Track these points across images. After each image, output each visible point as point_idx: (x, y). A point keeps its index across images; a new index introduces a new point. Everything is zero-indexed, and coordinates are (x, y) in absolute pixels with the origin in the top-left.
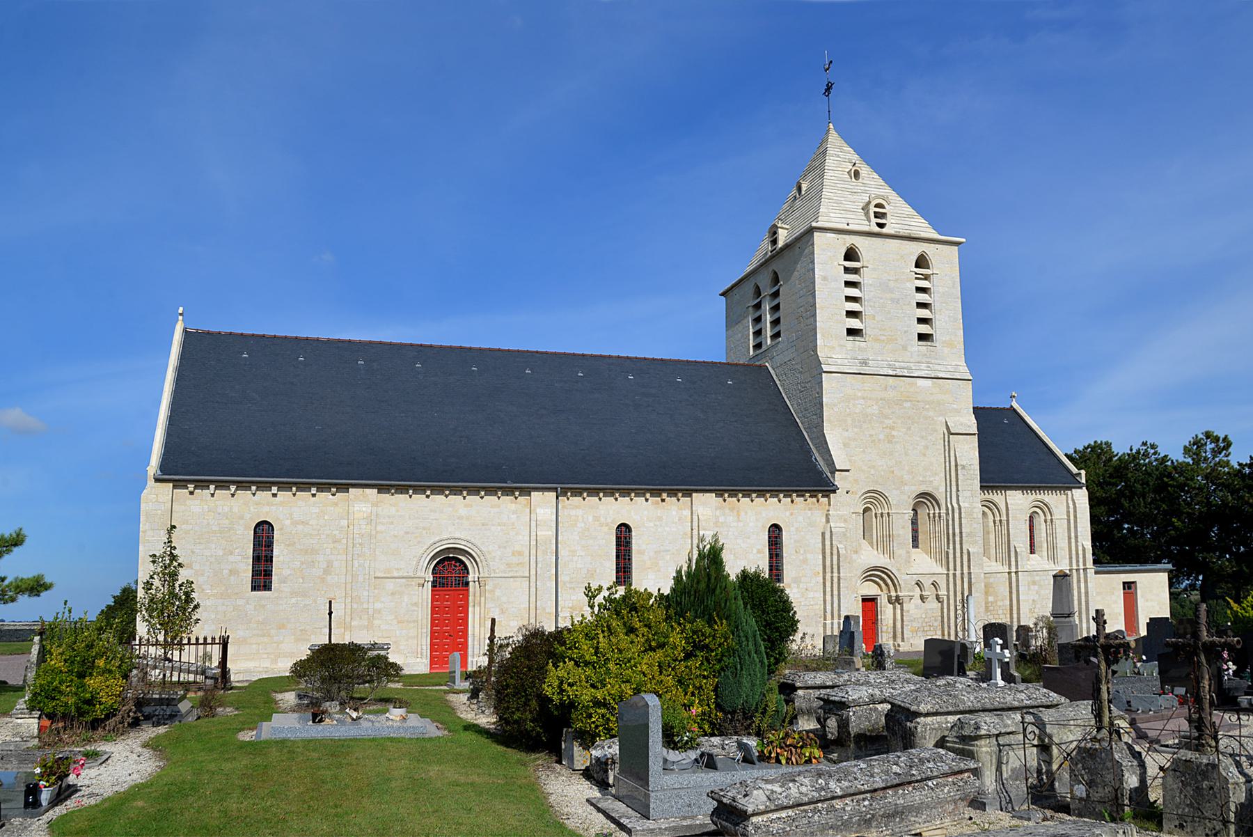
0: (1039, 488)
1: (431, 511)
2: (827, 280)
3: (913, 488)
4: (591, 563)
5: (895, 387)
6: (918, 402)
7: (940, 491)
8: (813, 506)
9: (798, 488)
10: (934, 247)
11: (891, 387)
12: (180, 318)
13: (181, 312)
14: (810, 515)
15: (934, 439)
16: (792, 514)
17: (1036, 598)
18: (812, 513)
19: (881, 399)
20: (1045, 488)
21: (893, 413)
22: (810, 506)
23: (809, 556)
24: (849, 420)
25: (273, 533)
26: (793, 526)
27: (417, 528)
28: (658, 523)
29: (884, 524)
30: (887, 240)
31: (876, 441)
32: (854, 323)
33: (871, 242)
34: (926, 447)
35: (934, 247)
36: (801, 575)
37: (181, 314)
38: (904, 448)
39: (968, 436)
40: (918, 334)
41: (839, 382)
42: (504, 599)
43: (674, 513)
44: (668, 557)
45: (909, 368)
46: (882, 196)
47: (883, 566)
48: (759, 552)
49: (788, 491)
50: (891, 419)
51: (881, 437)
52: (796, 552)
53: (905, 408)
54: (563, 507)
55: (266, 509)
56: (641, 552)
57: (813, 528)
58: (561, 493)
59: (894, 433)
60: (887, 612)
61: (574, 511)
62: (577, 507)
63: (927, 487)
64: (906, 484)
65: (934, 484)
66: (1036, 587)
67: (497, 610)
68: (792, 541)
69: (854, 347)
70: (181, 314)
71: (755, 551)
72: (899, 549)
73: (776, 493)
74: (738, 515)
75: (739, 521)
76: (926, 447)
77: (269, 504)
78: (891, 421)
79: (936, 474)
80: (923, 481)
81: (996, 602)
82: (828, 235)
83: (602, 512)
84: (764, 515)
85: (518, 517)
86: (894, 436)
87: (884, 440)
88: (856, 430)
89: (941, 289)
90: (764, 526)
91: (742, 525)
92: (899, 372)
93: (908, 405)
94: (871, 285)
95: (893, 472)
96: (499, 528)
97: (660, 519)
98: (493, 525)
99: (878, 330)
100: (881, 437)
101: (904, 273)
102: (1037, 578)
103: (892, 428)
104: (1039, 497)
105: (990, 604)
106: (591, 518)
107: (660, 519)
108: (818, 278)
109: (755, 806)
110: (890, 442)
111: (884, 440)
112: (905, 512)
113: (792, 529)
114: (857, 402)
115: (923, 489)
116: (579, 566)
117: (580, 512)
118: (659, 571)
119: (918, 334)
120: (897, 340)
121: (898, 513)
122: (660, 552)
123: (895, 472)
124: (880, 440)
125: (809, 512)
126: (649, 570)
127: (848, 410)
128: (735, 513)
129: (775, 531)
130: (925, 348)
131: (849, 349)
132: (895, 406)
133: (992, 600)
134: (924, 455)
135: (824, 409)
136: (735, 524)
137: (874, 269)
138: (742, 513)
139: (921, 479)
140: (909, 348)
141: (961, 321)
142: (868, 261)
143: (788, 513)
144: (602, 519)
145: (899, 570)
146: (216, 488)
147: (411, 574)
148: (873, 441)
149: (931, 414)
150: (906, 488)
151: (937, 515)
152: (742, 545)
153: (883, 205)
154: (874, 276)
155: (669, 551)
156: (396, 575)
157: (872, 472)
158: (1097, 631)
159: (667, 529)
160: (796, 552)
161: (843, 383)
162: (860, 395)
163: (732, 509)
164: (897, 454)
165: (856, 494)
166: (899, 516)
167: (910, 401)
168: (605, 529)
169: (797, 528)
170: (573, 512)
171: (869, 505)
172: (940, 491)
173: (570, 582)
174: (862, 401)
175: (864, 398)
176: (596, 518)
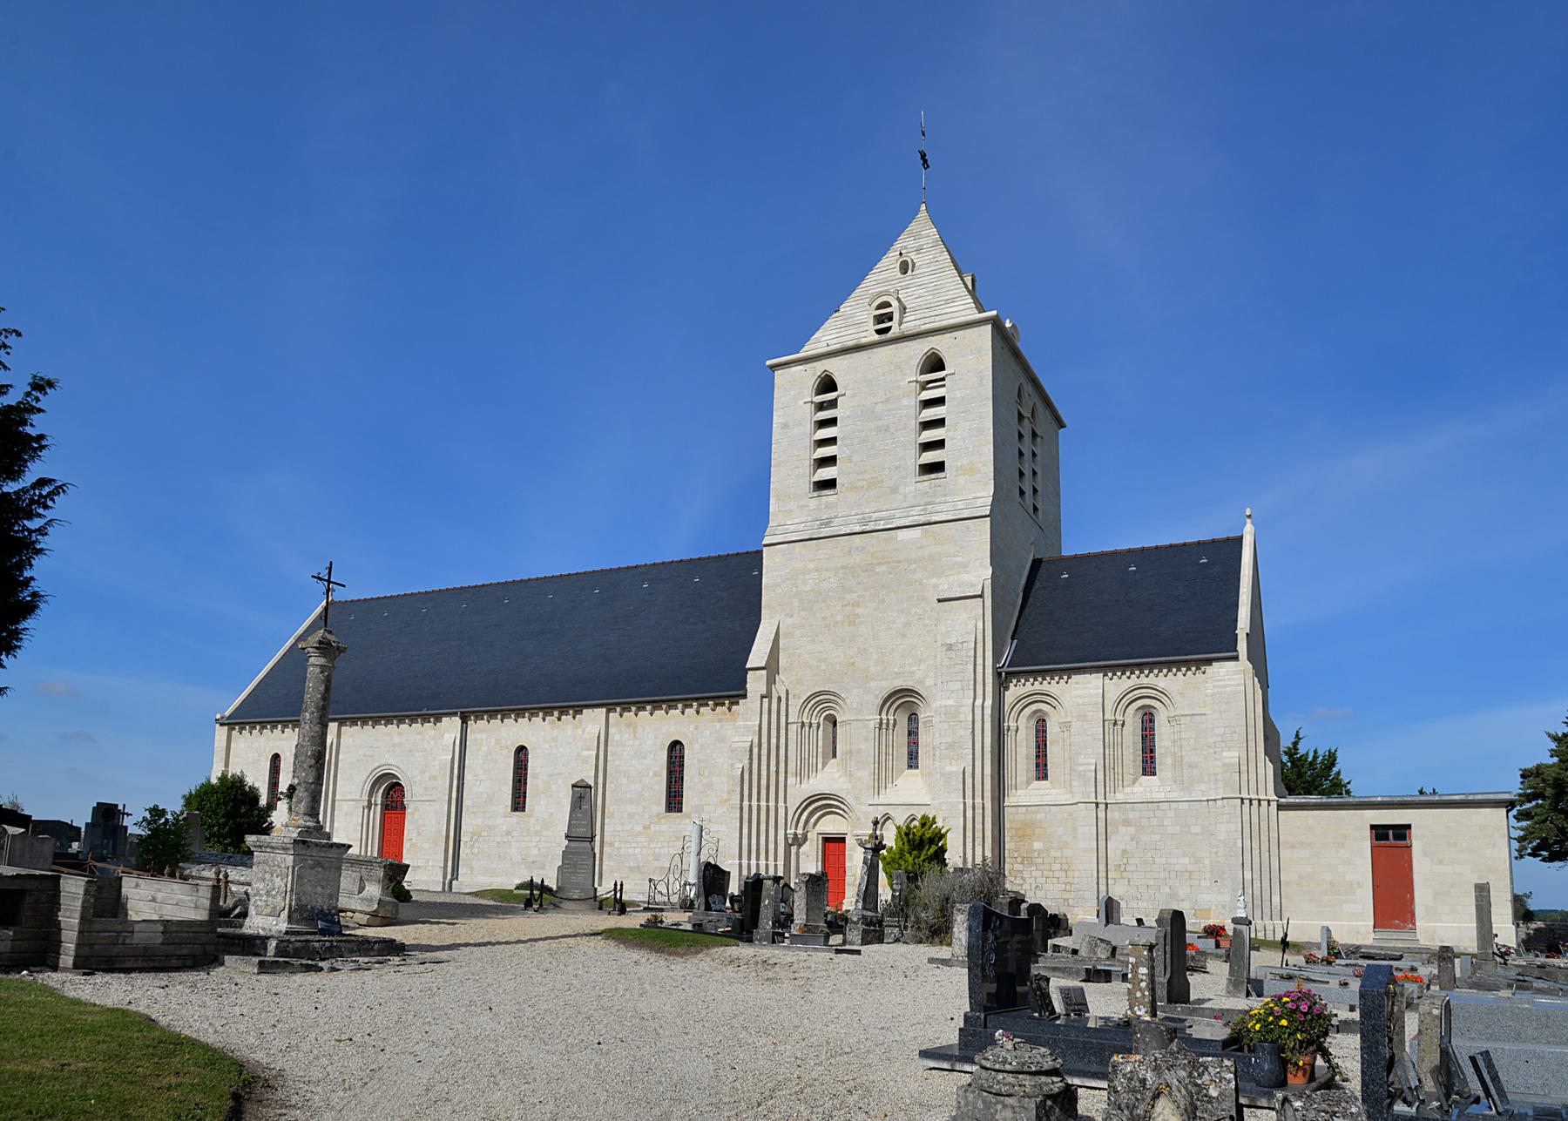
0: (1140, 666)
1: (375, 740)
2: (788, 428)
3: (884, 684)
4: (491, 788)
5: (864, 548)
6: (899, 562)
7: (927, 684)
8: (723, 717)
9: (699, 695)
10: (951, 337)
11: (857, 548)
12: (1248, 521)
13: (1248, 514)
14: (718, 728)
15: (920, 612)
16: (697, 728)
17: (1131, 846)
18: (721, 727)
19: (842, 568)
20: (1151, 666)
21: (859, 583)
22: (720, 717)
23: (715, 779)
24: (796, 603)
25: (1037, 741)
26: (697, 743)
27: (365, 756)
28: (553, 744)
29: (807, 741)
30: (875, 350)
31: (832, 625)
32: (826, 473)
33: (852, 360)
34: (908, 624)
35: (951, 337)
36: (704, 803)
37: (1249, 517)
38: (873, 630)
39: (969, 601)
40: (944, 462)
41: (783, 555)
42: (420, 822)
43: (569, 732)
44: (560, 781)
45: (892, 518)
46: (886, 291)
47: (832, 793)
48: (656, 774)
49: (673, 700)
50: (856, 592)
51: (839, 618)
52: (700, 774)
53: (878, 574)
54: (472, 731)
55: (278, 743)
56: (536, 776)
57: (722, 745)
58: (610, 708)
59: (858, 610)
60: (855, 857)
61: (480, 735)
62: (483, 731)
63: (904, 681)
64: (872, 679)
65: (917, 676)
66: (1132, 830)
67: (415, 832)
68: (695, 761)
69: (820, 504)
70: (1249, 517)
71: (651, 774)
72: (858, 769)
73: (674, 704)
74: (635, 732)
75: (635, 738)
76: (908, 624)
77: (280, 739)
78: (856, 594)
79: (920, 661)
80: (900, 673)
81: (1048, 850)
82: (794, 369)
83: (504, 735)
84: (664, 731)
85: (436, 743)
86: (858, 615)
87: (843, 622)
88: (804, 613)
89: (958, 394)
90: (663, 744)
91: (639, 743)
92: (871, 527)
93: (881, 569)
94: (848, 417)
95: (853, 664)
96: (421, 753)
97: (555, 739)
98: (417, 751)
99: (855, 475)
100: (839, 618)
101: (899, 387)
102: (1131, 815)
103: (857, 604)
104: (1144, 680)
105: (1036, 854)
106: (493, 741)
107: (555, 739)
108: (776, 428)
109: (968, 1094)
110: (852, 624)
111: (843, 622)
112: (868, 718)
113: (696, 746)
114: (807, 577)
115: (899, 683)
116: (481, 790)
117: (484, 735)
118: (551, 796)
119: (944, 462)
120: (882, 481)
121: (859, 720)
122: (553, 775)
123: (857, 664)
124: (837, 623)
125: (718, 725)
126: (542, 795)
127: (794, 589)
128: (632, 730)
129: (676, 748)
130: (926, 484)
131: (811, 508)
132: (863, 574)
133: (1041, 847)
134: (904, 636)
135: (763, 593)
136: (631, 742)
137: (853, 396)
138: (640, 729)
139: (896, 670)
140: (902, 489)
141: (992, 431)
142: (845, 387)
143: (692, 727)
144: (503, 742)
145: (856, 798)
146: (700, 705)
147: (358, 798)
148: (827, 626)
149: (919, 575)
150: (873, 684)
151: (885, 721)
152: (637, 766)
153: (889, 302)
154: (853, 404)
155: (561, 774)
156: (349, 798)
157: (823, 666)
158: (416, 901)
159: (561, 750)
160: (700, 774)
161: (789, 556)
162: (812, 566)
163: (629, 725)
164: (862, 639)
165: (799, 698)
166: (860, 724)
167: (885, 563)
168: (505, 752)
169: (702, 745)
170: (479, 736)
171: (827, 713)
172: (927, 684)
173: (472, 807)
174: (815, 575)
175: (817, 570)
176: (498, 741)
